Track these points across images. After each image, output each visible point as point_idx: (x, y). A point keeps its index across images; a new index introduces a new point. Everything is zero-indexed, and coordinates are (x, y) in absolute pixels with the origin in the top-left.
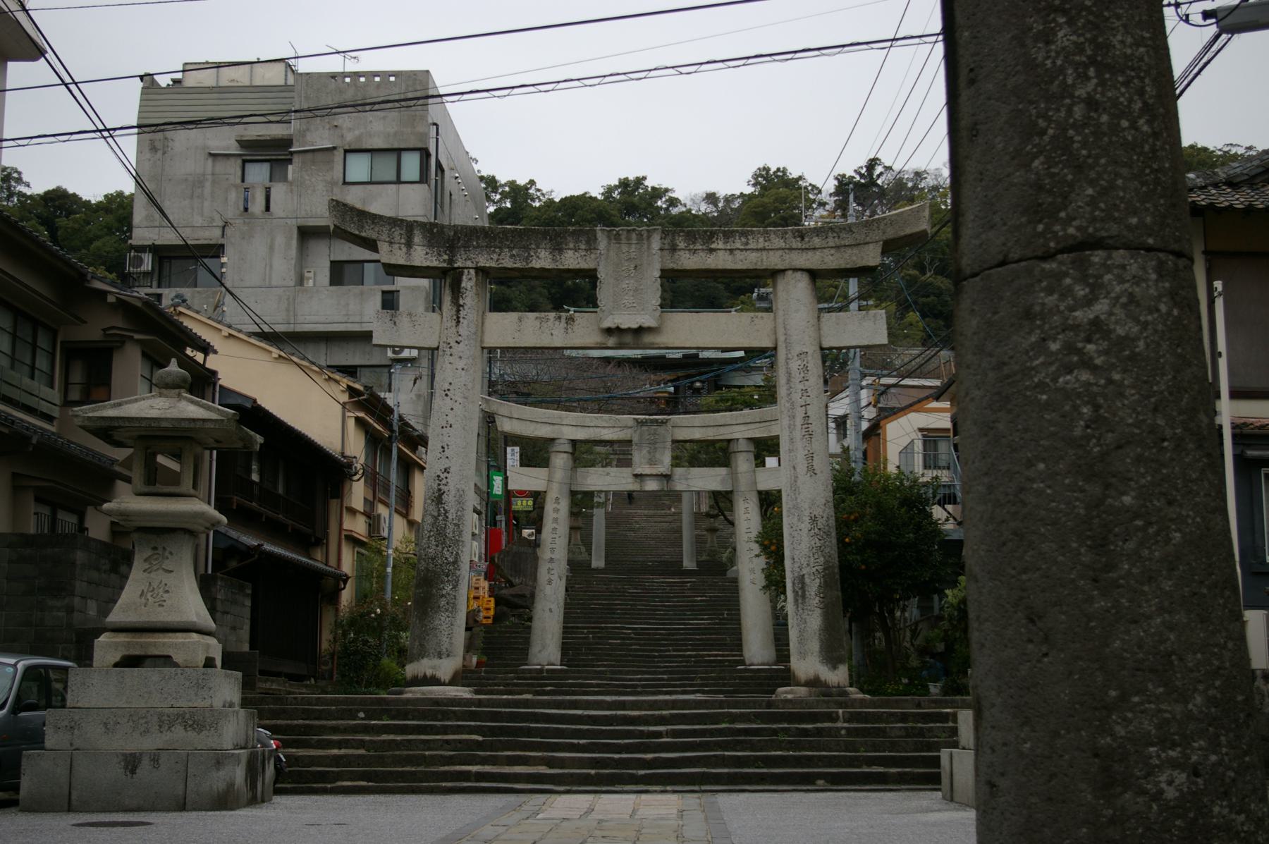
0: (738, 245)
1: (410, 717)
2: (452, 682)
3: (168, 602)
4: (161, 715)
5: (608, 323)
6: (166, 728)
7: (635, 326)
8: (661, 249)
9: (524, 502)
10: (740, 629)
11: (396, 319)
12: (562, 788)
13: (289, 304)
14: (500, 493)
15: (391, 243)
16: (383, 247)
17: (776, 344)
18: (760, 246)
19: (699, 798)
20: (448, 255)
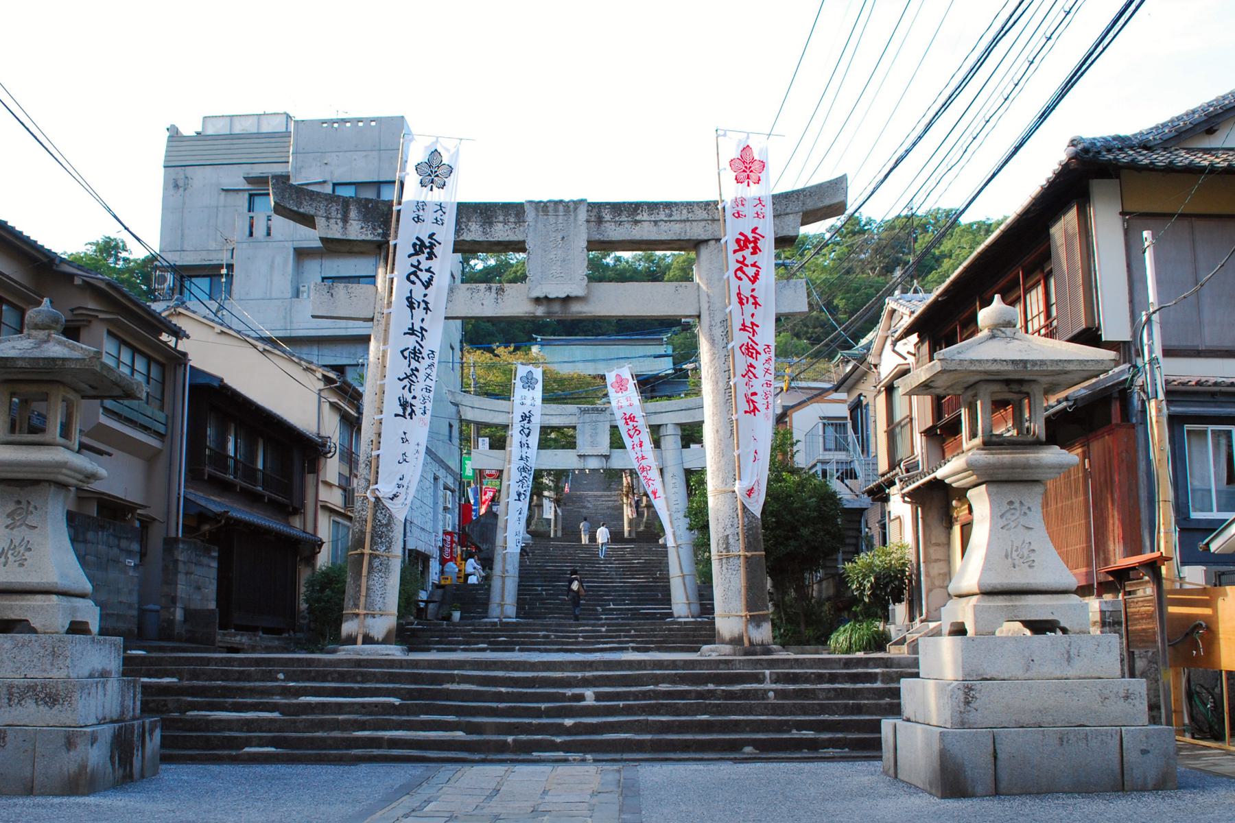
0: (662, 217)
1: (330, 679)
2: (386, 641)
3: (29, 561)
4: (10, 687)
5: (538, 292)
6: (16, 701)
7: (563, 295)
8: (588, 221)
10: (669, 586)
11: (332, 291)
12: (477, 757)
13: (286, 313)
14: (471, 475)
15: (328, 218)
16: (320, 222)
17: (700, 313)
18: (684, 217)
19: (619, 771)
20: (382, 229)
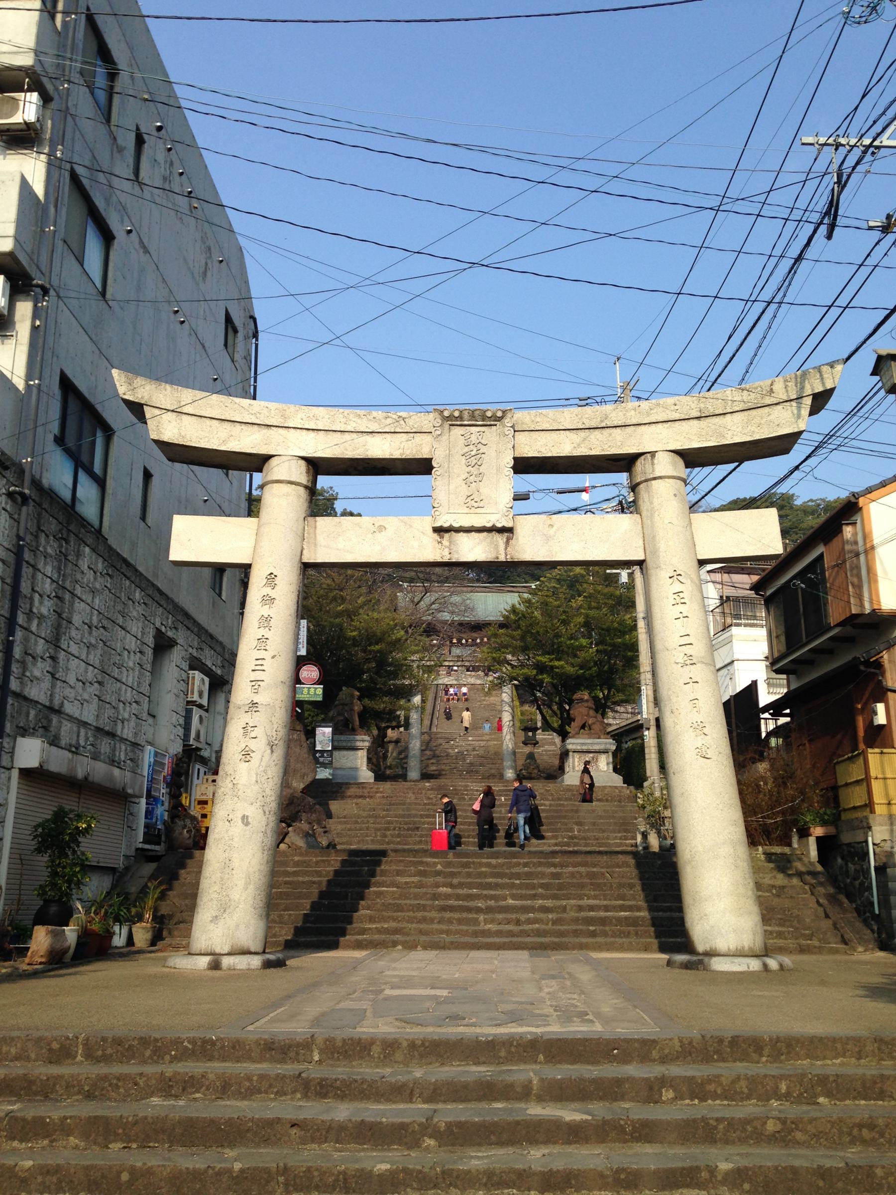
9: (312, 690)
